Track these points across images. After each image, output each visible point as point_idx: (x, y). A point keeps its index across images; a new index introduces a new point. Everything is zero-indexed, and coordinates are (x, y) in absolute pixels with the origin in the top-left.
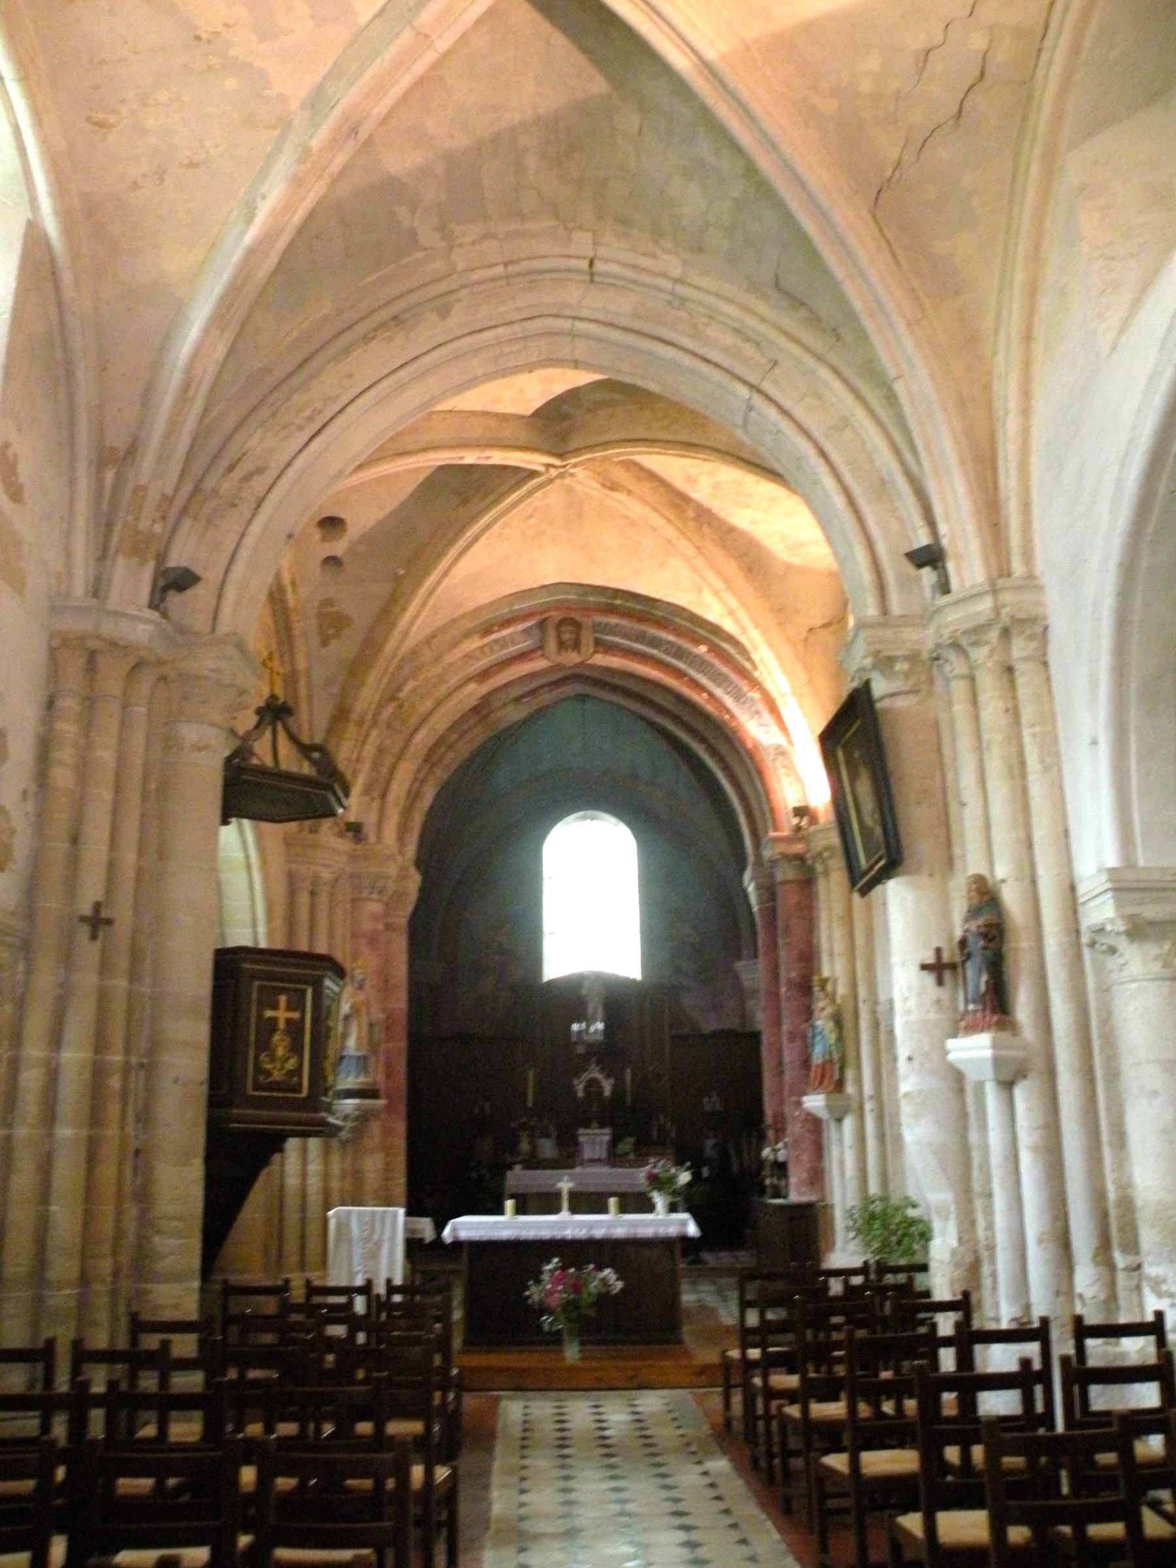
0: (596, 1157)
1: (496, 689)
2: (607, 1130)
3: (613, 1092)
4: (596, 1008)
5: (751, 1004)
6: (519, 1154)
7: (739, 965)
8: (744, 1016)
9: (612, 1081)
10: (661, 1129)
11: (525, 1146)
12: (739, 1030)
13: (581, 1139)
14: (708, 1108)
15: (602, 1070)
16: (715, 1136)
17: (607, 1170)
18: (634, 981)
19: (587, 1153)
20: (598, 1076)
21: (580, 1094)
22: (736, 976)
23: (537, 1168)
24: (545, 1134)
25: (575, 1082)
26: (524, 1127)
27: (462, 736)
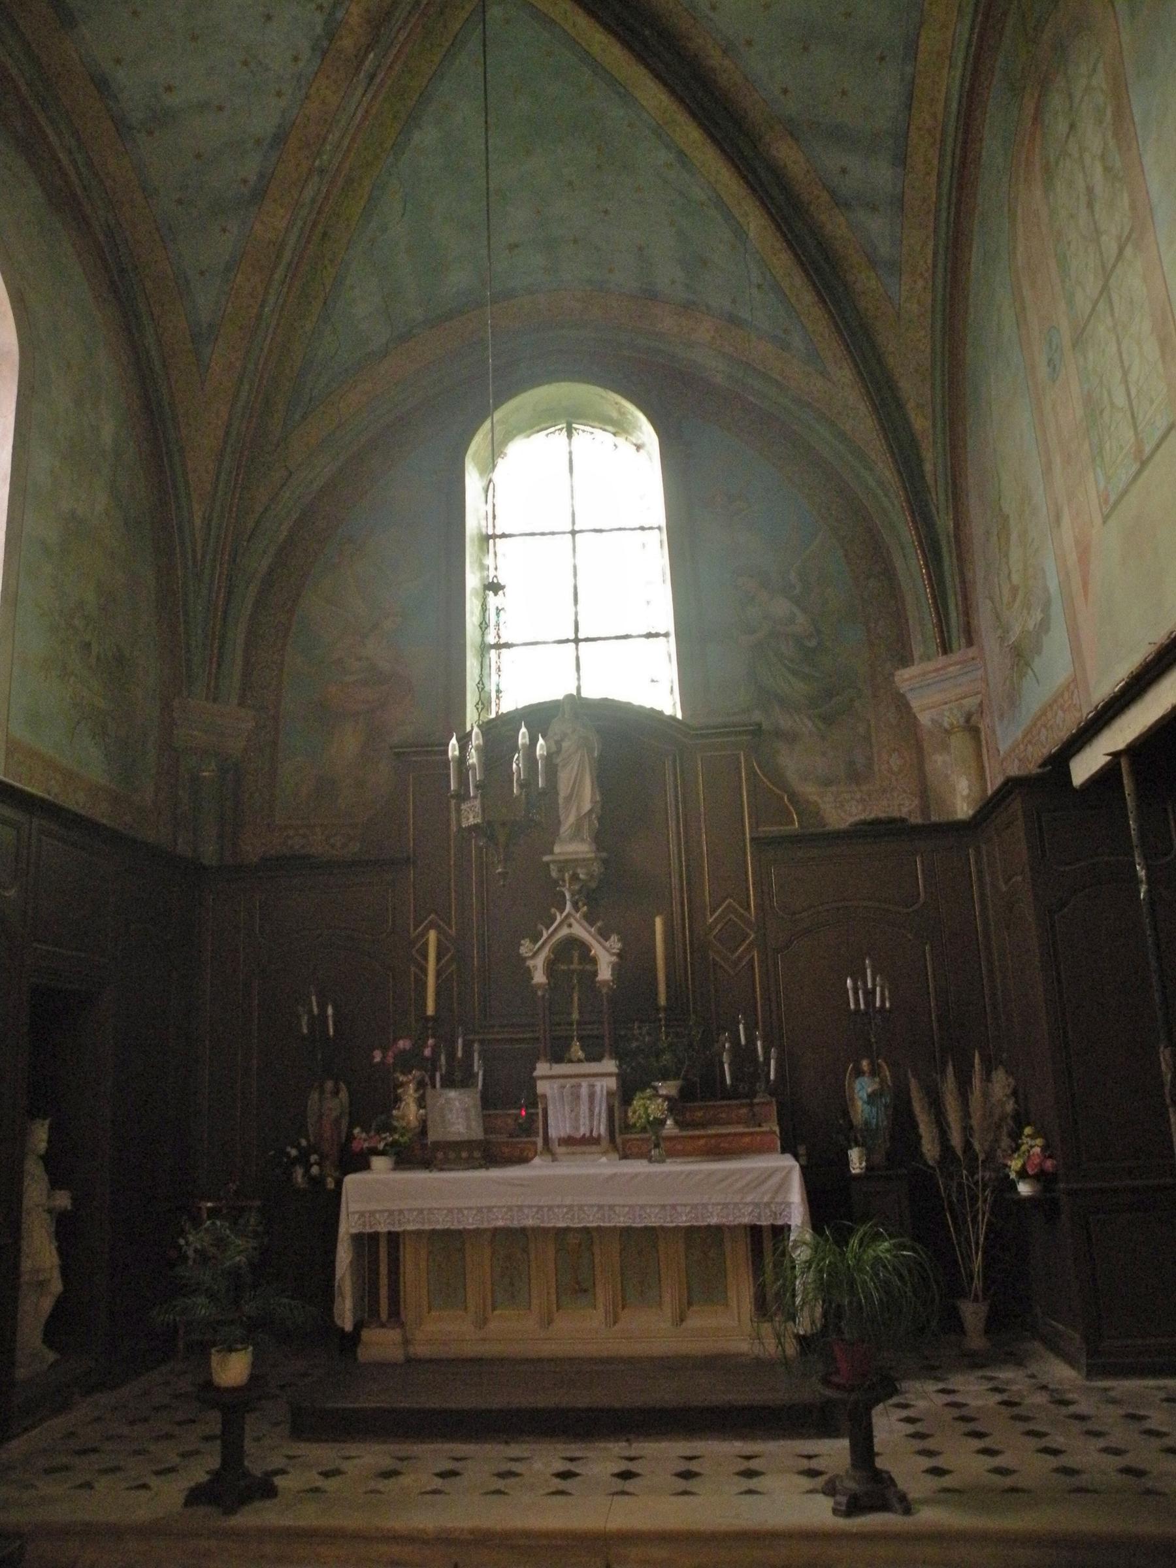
0: (583, 1130)
1: (547, 1126)
2: (610, 1065)
3: (617, 969)
4: (577, 783)
5: (938, 761)
6: (388, 1128)
7: (905, 677)
8: (924, 792)
9: (615, 943)
10: (744, 1057)
11: (409, 1111)
12: (916, 819)
13: (542, 1087)
14: (855, 1001)
15: (590, 919)
16: (875, 1072)
17: (605, 1166)
18: (655, 716)
19: (559, 1125)
20: (580, 930)
21: (539, 977)
22: (902, 705)
23: (427, 1164)
24: (458, 1078)
25: (526, 948)
26: (406, 1062)
27: (609, 1339)
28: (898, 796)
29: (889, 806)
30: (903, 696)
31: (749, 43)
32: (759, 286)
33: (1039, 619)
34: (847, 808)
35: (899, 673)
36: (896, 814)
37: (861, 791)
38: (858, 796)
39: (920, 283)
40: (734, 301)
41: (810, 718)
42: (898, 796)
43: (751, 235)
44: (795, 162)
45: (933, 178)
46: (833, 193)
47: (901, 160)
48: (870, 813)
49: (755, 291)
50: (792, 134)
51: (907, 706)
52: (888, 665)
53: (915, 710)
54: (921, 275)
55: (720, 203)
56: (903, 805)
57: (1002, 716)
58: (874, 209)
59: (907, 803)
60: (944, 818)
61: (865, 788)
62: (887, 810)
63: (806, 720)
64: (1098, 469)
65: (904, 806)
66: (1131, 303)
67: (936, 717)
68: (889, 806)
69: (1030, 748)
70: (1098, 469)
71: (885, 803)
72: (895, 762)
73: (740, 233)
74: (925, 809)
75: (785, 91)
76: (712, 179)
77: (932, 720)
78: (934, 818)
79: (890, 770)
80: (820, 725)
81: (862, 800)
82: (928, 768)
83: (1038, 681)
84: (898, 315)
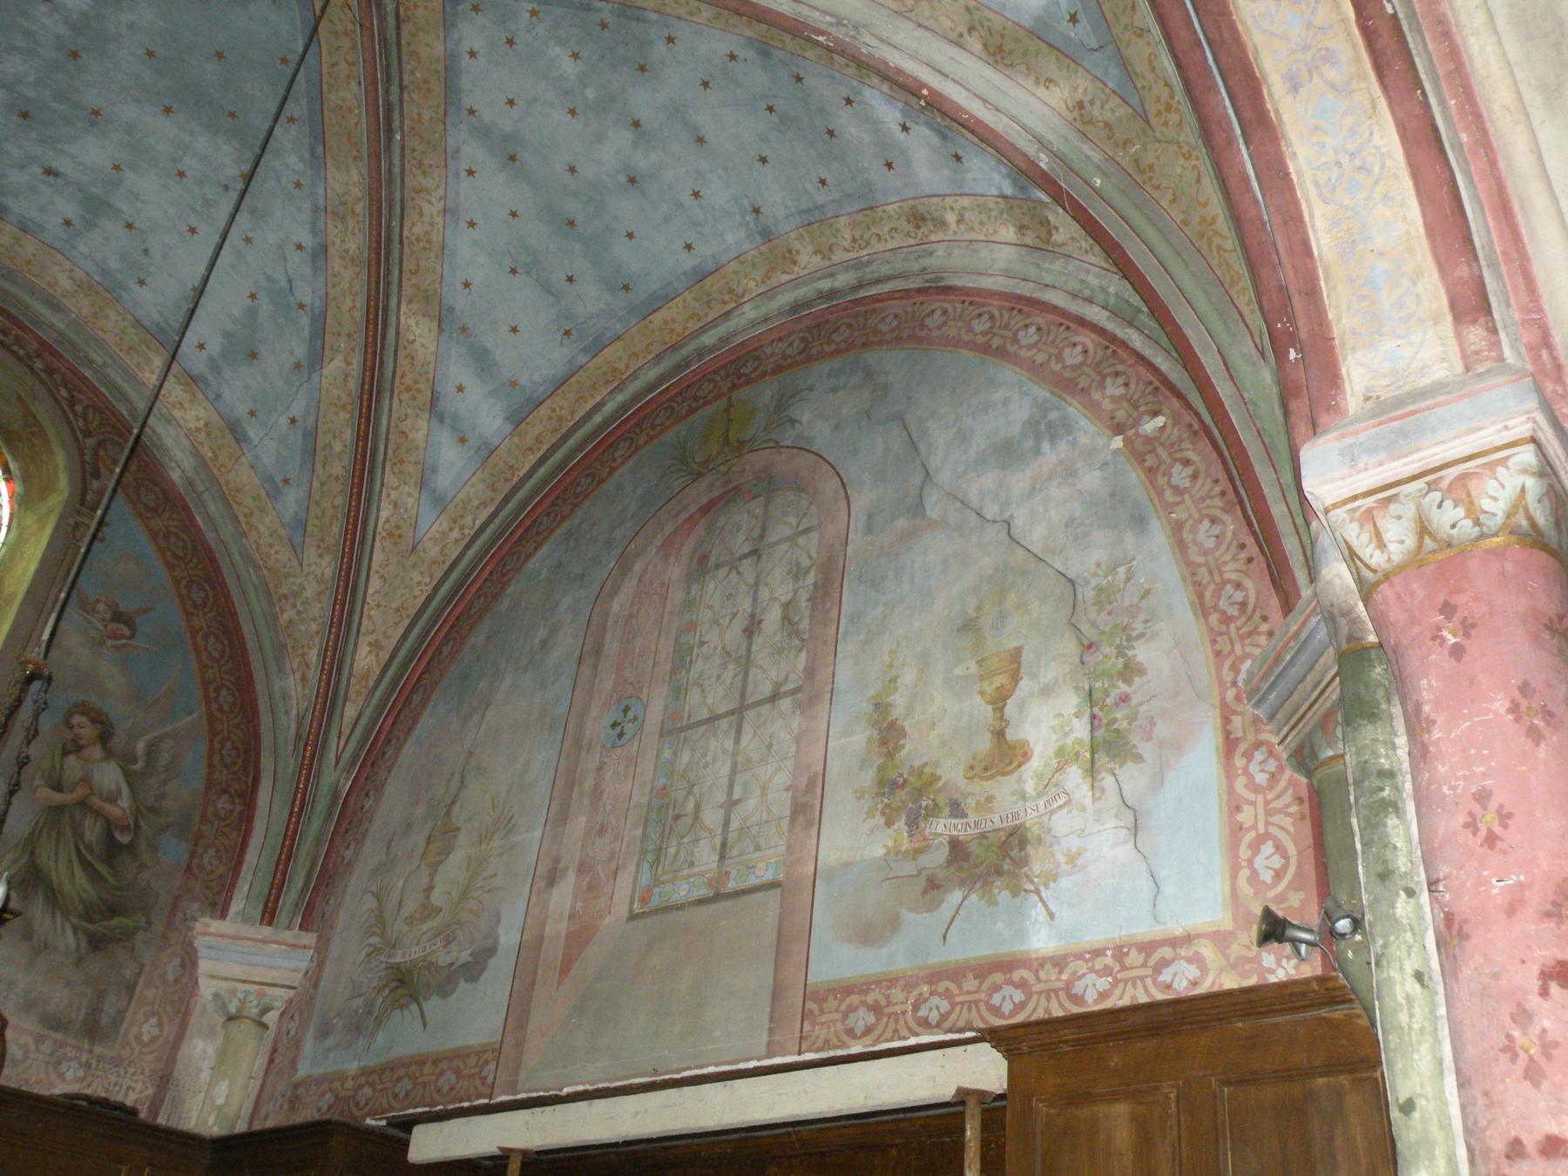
8: (164, 1080)
28: (133, 1075)
29: (116, 1085)
30: (195, 950)
31: (472, 224)
32: (293, 421)
33: (462, 961)
34: (63, 1068)
35: (206, 920)
36: (119, 1098)
37: (91, 1052)
38: (85, 1057)
39: (456, 534)
40: (252, 414)
41: (75, 930)
42: (133, 1075)
43: (325, 371)
44: (422, 345)
45: (533, 458)
46: (434, 399)
47: (518, 419)
48: (89, 1086)
49: (284, 421)
50: (440, 321)
51: (194, 965)
52: (196, 906)
53: (201, 971)
54: (462, 528)
55: (320, 323)
56: (133, 1089)
57: (323, 1033)
58: (462, 440)
59: (139, 1086)
60: (173, 1124)
61: (98, 1049)
62: (111, 1088)
63: (69, 932)
64: (646, 866)
65: (132, 1090)
66: (769, 747)
67: (223, 993)
68: (116, 1085)
69: (367, 1091)
70: (646, 866)
71: (113, 1078)
72: (149, 1029)
73: (316, 358)
74: (156, 1105)
75: (467, 285)
76: (332, 292)
77: (217, 995)
78: (161, 1120)
79: (138, 1038)
80: (83, 944)
81: (87, 1065)
82: (184, 1051)
83: (425, 1025)
84: (414, 548)
